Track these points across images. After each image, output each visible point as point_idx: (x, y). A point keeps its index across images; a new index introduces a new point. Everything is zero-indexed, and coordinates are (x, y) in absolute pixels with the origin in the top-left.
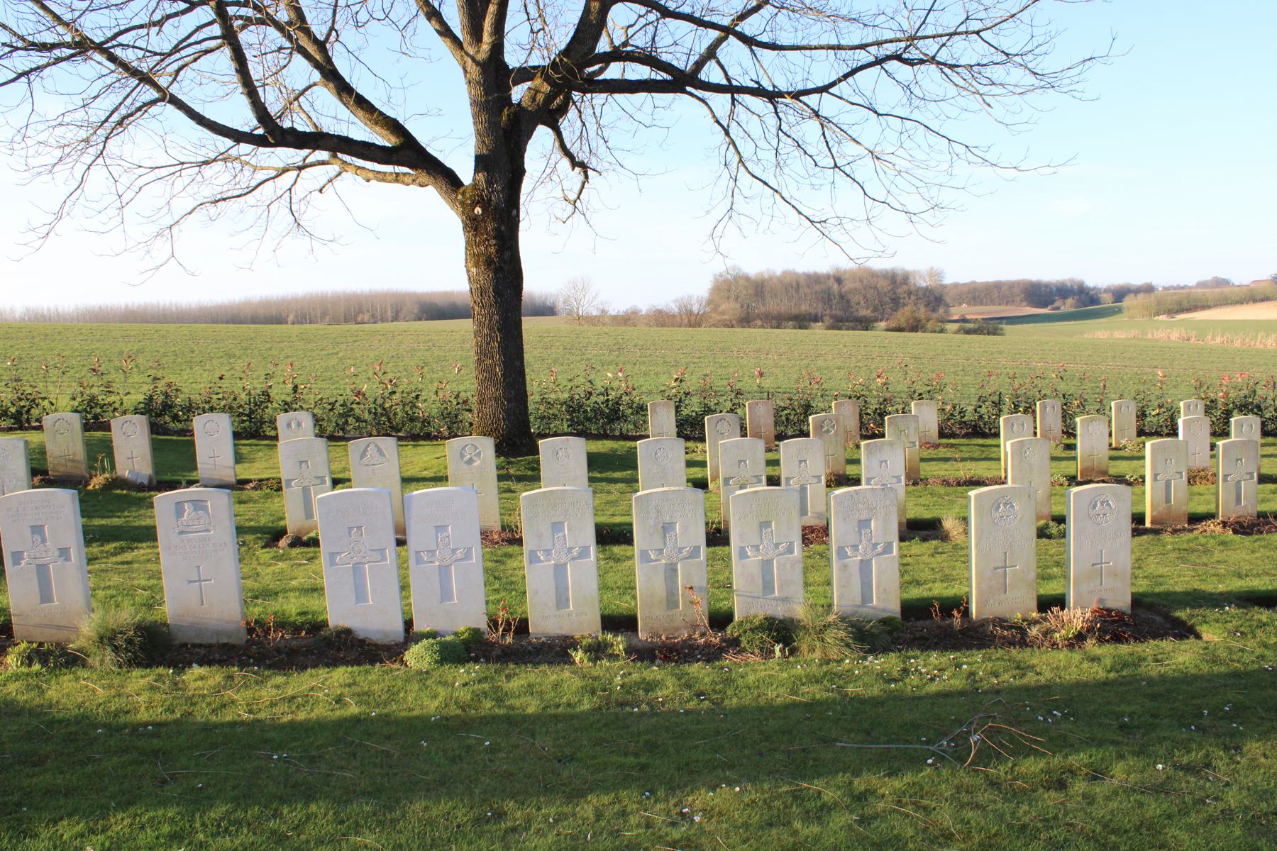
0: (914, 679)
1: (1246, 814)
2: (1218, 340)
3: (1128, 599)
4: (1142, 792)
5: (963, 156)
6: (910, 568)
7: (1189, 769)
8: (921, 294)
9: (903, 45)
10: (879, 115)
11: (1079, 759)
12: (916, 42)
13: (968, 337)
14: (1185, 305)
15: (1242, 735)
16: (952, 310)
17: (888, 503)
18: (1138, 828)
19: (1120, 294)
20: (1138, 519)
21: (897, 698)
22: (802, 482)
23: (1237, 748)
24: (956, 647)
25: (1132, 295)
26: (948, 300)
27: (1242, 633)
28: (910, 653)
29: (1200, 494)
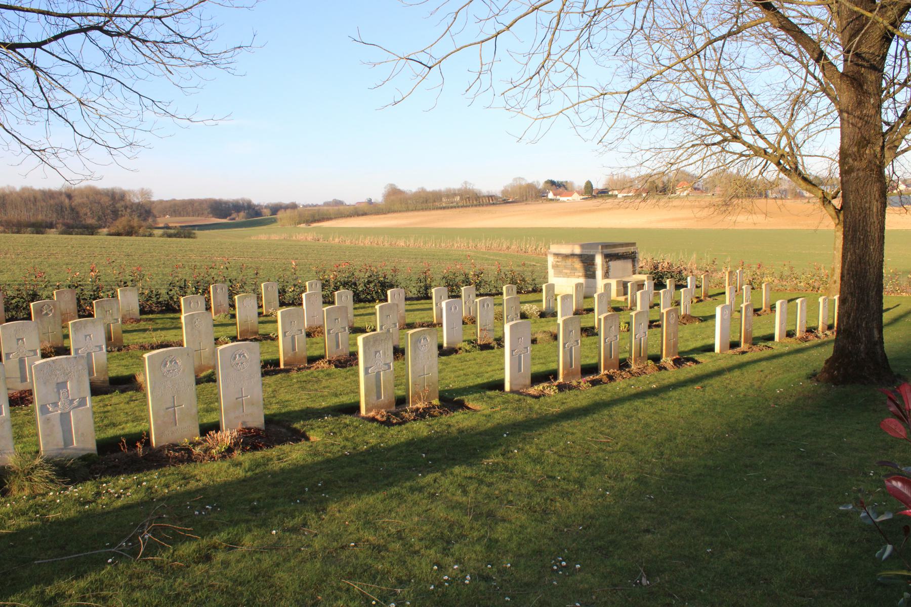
0: (105, 499)
1: (324, 552)
2: (337, 240)
3: (262, 420)
4: (261, 552)
5: (150, 108)
6: (109, 414)
7: (294, 530)
8: (134, 208)
9: (102, 19)
10: (84, 71)
11: (220, 538)
12: (114, 18)
13: (169, 239)
14: (317, 217)
15: (327, 500)
16: (159, 220)
17: (80, 367)
18: (256, 578)
19: (276, 209)
20: (440, 347)
21: (89, 516)
22: (21, 356)
23: (324, 510)
24: (139, 470)
25: (283, 210)
26: (155, 212)
27: (334, 433)
28: (103, 479)
29: (317, 343)
